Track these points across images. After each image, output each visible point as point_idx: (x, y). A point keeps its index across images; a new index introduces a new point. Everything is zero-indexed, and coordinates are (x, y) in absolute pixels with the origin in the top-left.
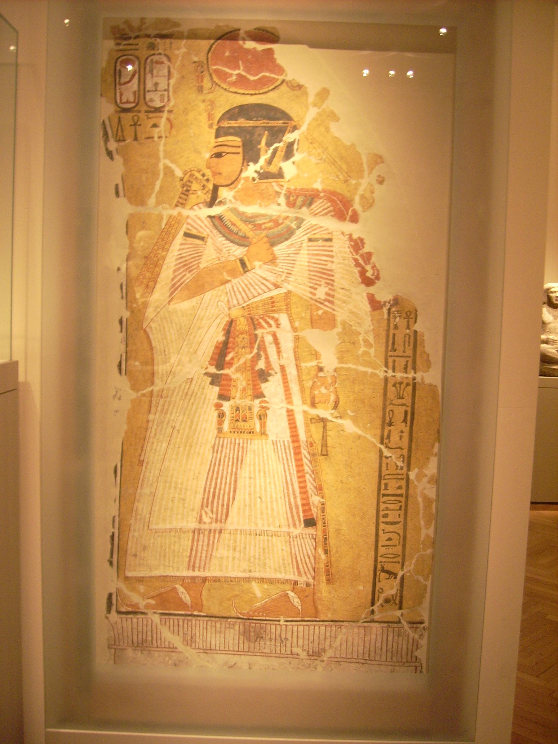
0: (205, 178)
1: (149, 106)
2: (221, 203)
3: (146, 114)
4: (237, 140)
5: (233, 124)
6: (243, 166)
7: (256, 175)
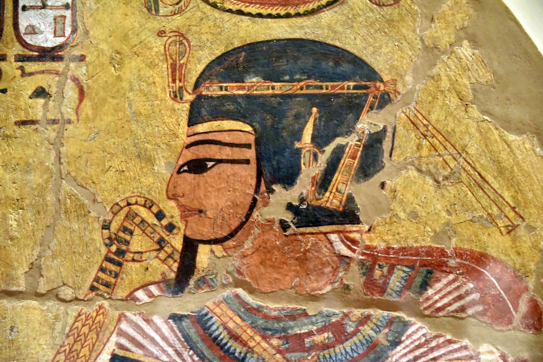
0: (164, 222)
1: (25, 45)
2: (203, 282)
3: (20, 64)
4: (240, 130)
5: (234, 89)
6: (257, 191)
7: (288, 217)
